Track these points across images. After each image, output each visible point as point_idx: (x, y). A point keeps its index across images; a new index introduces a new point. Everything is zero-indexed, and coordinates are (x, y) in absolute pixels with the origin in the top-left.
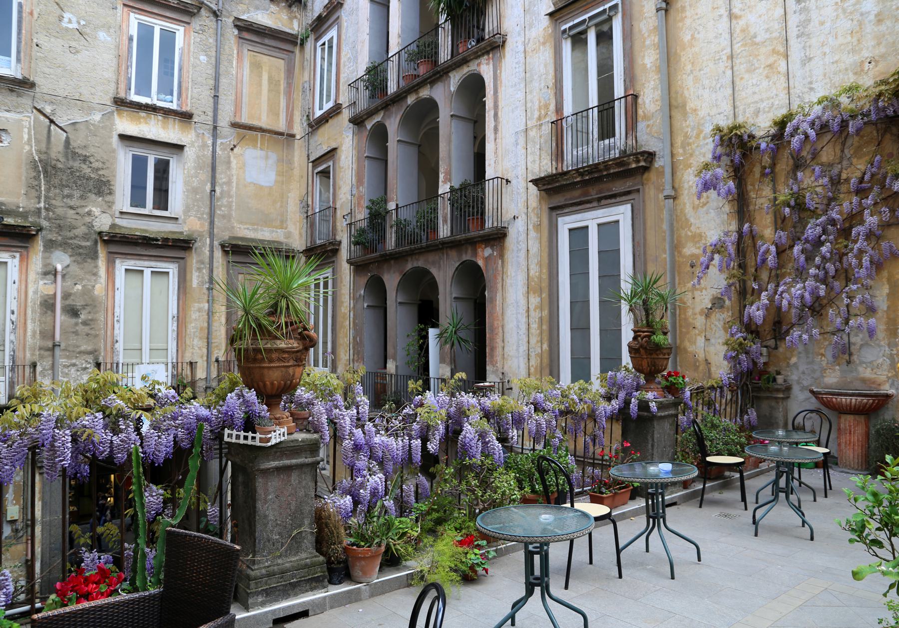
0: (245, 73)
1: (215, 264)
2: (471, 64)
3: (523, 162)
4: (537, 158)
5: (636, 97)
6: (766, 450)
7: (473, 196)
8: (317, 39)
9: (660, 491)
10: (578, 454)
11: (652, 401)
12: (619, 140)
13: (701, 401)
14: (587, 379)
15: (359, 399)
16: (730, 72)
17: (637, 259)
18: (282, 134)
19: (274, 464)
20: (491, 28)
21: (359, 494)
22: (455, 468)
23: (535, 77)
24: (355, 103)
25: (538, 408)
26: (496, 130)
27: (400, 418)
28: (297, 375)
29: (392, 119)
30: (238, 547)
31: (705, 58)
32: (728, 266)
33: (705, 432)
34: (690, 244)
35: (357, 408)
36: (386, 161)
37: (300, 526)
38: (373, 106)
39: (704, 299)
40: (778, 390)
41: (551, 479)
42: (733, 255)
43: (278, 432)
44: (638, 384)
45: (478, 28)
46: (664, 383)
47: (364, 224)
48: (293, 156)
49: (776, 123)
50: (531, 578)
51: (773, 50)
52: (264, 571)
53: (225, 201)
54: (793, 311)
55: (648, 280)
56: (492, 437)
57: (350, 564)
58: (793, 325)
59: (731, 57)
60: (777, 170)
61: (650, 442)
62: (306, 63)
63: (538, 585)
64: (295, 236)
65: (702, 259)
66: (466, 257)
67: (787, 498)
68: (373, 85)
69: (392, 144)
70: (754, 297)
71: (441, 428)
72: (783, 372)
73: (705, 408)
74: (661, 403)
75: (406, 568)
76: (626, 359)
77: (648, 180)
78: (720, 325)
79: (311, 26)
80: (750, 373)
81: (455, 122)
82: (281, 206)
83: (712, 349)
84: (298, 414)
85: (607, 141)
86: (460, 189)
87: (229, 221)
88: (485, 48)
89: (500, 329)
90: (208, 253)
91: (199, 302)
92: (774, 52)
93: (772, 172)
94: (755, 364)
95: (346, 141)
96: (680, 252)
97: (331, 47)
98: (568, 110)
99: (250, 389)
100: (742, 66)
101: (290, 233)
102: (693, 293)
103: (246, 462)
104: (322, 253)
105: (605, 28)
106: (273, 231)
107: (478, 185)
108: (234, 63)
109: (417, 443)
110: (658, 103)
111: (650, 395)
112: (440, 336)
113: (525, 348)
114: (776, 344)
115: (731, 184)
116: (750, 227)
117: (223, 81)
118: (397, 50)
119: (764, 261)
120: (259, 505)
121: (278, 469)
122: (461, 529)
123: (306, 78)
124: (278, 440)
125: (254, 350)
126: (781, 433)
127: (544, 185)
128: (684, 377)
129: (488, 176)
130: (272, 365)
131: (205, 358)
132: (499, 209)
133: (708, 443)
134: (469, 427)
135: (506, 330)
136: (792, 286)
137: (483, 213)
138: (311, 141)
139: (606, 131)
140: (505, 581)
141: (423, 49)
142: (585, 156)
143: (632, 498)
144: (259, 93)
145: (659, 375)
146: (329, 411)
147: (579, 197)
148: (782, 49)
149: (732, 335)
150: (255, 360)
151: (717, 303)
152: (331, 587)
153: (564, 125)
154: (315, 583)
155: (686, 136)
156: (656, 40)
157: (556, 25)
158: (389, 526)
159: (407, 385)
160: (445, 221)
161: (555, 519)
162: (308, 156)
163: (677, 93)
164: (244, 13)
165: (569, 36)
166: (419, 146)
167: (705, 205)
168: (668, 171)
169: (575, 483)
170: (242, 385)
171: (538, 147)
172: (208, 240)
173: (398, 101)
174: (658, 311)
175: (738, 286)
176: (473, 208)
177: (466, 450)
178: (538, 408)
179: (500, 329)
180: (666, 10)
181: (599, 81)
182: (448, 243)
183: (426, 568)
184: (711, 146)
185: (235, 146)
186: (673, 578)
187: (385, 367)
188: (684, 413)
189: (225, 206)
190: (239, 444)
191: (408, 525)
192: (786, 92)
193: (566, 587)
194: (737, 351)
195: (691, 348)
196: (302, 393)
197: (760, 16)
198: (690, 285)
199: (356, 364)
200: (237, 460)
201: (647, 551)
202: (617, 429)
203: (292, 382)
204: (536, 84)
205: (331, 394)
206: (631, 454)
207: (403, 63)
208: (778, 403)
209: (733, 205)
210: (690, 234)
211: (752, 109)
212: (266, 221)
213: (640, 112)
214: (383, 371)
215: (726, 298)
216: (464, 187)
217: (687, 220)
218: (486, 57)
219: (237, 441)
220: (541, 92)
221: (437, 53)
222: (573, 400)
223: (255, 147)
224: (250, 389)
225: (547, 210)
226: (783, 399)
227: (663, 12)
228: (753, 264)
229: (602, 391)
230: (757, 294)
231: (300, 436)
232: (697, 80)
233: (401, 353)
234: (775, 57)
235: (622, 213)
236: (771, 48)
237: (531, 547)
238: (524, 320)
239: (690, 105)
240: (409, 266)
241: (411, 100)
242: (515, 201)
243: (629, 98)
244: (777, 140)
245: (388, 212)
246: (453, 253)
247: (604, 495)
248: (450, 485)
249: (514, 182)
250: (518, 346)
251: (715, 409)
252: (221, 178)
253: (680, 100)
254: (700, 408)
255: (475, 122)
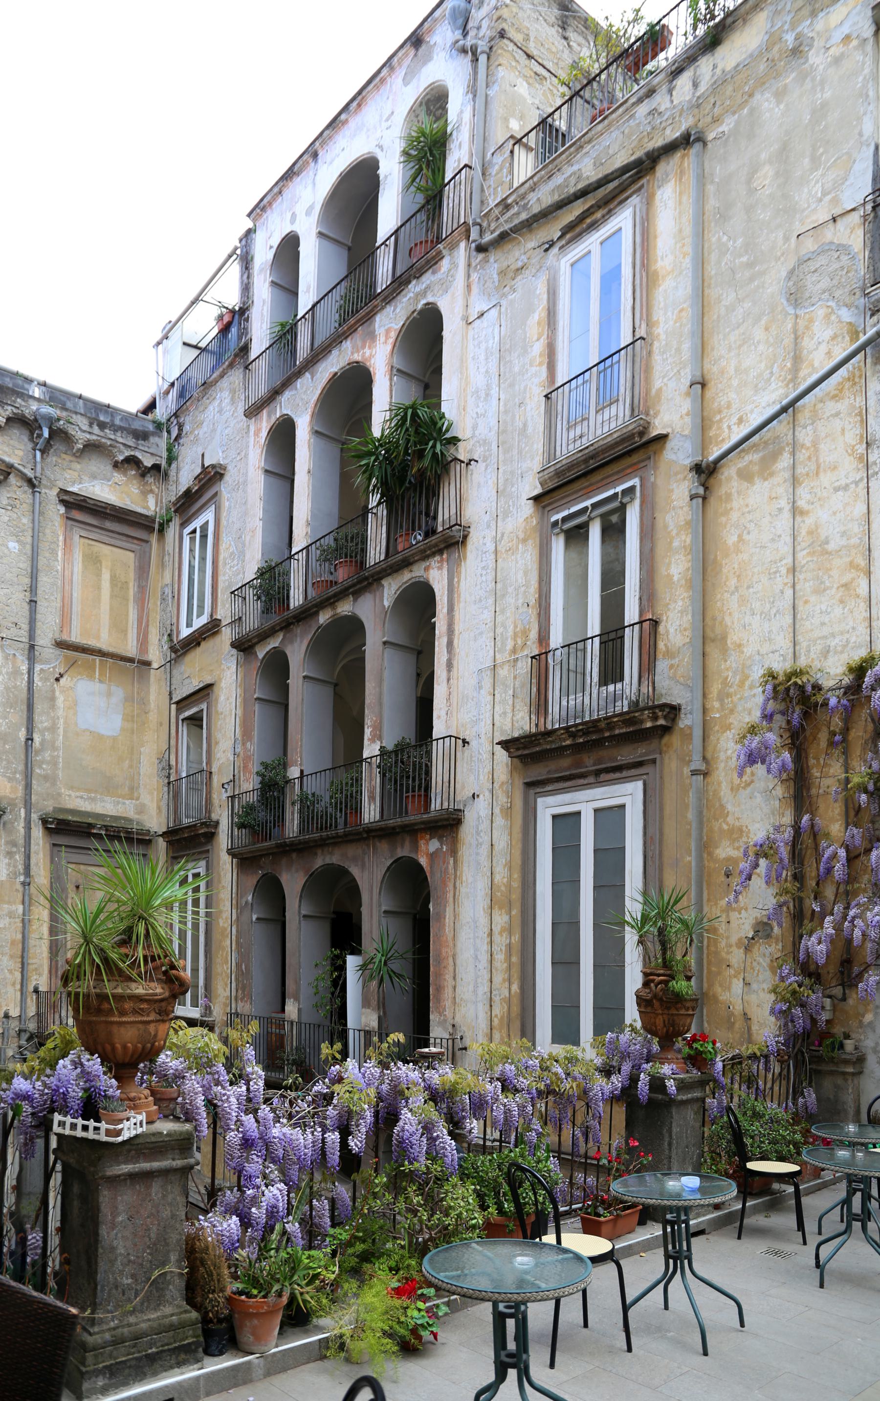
0: (76, 570)
1: (33, 848)
2: (415, 567)
3: (488, 715)
4: (509, 709)
5: (655, 623)
6: (832, 1157)
7: (414, 763)
8: (183, 525)
9: (683, 1218)
10: (563, 1149)
11: (670, 1078)
12: (630, 684)
13: (737, 1078)
14: (576, 1041)
15: (249, 1070)
16: (791, 591)
17: (649, 862)
18: (131, 660)
19: (126, 1168)
20: (446, 516)
21: (250, 1213)
22: (388, 1176)
23: (510, 590)
24: (240, 618)
25: (507, 1086)
26: (450, 665)
27: (309, 1098)
28: (161, 1034)
29: (296, 645)
30: (74, 1311)
31: (756, 570)
32: (779, 876)
33: (745, 1124)
34: (725, 843)
35: (247, 1084)
36: (286, 706)
37: (163, 1264)
38: (268, 625)
39: (743, 924)
40: (846, 1062)
41: (527, 1194)
42: (786, 861)
43: (133, 1121)
44: (649, 1051)
45: (427, 515)
46: (687, 1050)
47: (253, 798)
48: (148, 693)
49: (851, 670)
50: (503, 1353)
51: (851, 563)
52: (107, 1336)
53: (47, 755)
54: (869, 945)
55: (666, 898)
56: (442, 1131)
57: (236, 1323)
58: (867, 967)
59: (793, 570)
60: (850, 738)
61: (667, 1139)
62: (167, 558)
63: (513, 1366)
64: (154, 818)
65: (742, 865)
66: (403, 851)
67: (864, 1228)
68: (268, 594)
69: (295, 682)
70: (814, 924)
71: (369, 1115)
72: (853, 1035)
73: (744, 1087)
74: (682, 1081)
75: (320, 1329)
76: (632, 1013)
77: (668, 746)
78: (765, 962)
79: (174, 504)
80: (806, 1035)
81: (389, 652)
82: (131, 767)
83: (753, 998)
84: (163, 1093)
85: (611, 688)
86: (396, 752)
87: (54, 784)
88: (436, 545)
89: (451, 960)
90: (22, 831)
91: (9, 903)
92: (852, 565)
93: (844, 740)
94: (814, 1021)
95: (226, 675)
96: (710, 854)
97: (204, 537)
98: (556, 639)
99: (92, 1054)
100: (807, 585)
101: (143, 805)
102: (728, 916)
103: (83, 1164)
104: (189, 840)
105: (614, 519)
106: (118, 803)
107: (421, 746)
108: (60, 554)
109: (333, 1137)
110: (687, 633)
111: (666, 1069)
112: (363, 967)
113: (487, 989)
114: (844, 994)
115: (787, 756)
116: (811, 820)
117: (44, 580)
118: (304, 544)
119: (829, 870)
120: (103, 1231)
121: (133, 1177)
122: (397, 1270)
123: (167, 579)
124: (133, 1133)
125: (98, 996)
126: (852, 1128)
127: (518, 749)
128: (714, 1043)
129: (436, 734)
130: (124, 1019)
131: (18, 987)
132: (451, 782)
133: (748, 1141)
134: (409, 1115)
135: (458, 962)
136: (868, 909)
137: (428, 788)
138: (174, 672)
139: (612, 671)
140: (463, 1357)
141: (344, 544)
142: (579, 708)
143: (642, 1222)
144: (98, 599)
145: (680, 1039)
146: (207, 1089)
147: (569, 768)
148: (863, 563)
149: (782, 979)
150: (99, 1011)
151: (762, 930)
152: (207, 1360)
153: (550, 661)
154: (184, 1355)
155: (725, 683)
156: (688, 541)
157: (543, 514)
158: (293, 1264)
159: (320, 1049)
160: (372, 798)
161: (536, 1265)
162: (170, 694)
163: (714, 619)
164: (74, 483)
165: (562, 530)
166: (336, 685)
167: (748, 785)
168: (697, 733)
169: (559, 1197)
170: (80, 1048)
171: (511, 692)
172: (23, 811)
173: (305, 618)
174: (679, 945)
175: (792, 907)
176: (414, 780)
177: (405, 1150)
178: (507, 1086)
179: (451, 960)
180: (704, 498)
181: (602, 597)
182: (376, 830)
183: (347, 1330)
184: (760, 699)
185: (61, 675)
186: (705, 1353)
187: (283, 1010)
188: (714, 1093)
189: (48, 763)
190: (75, 1138)
191: (319, 1261)
192: (867, 624)
193: (552, 1365)
194: (789, 1003)
195: (723, 996)
196: (167, 1060)
197: (835, 513)
198: (723, 903)
199: (240, 1004)
200: (72, 1161)
201: (666, 1307)
202: (620, 1113)
203: (153, 1045)
204: (510, 600)
205: (210, 1064)
206: (639, 1156)
207: (313, 562)
208: (846, 1080)
209: (788, 788)
210: (725, 827)
211: (819, 647)
212: (109, 787)
213: (661, 645)
214: (280, 1015)
215: (775, 924)
216: (401, 748)
217: (722, 807)
218: (437, 558)
219: (73, 1133)
220: (518, 612)
221: (364, 551)
222: (556, 1074)
223: (91, 677)
224: (92, 1054)
225: (521, 786)
226: (853, 1074)
227: (700, 500)
228: (814, 874)
229: (598, 1061)
230: (818, 918)
231: (166, 1127)
232: (743, 601)
233: (306, 991)
234: (854, 573)
235: (629, 794)
236: (848, 560)
237: (501, 1307)
238: (485, 947)
239: (733, 638)
240: (319, 861)
241: (324, 618)
242: (475, 775)
243: (646, 625)
244: (853, 694)
245: (288, 782)
246: (383, 846)
247: (602, 1219)
248: (385, 1208)
249: (474, 743)
250: (476, 986)
251: (757, 1088)
252: (41, 720)
253: (718, 630)
254: (736, 1086)
255: (419, 653)
